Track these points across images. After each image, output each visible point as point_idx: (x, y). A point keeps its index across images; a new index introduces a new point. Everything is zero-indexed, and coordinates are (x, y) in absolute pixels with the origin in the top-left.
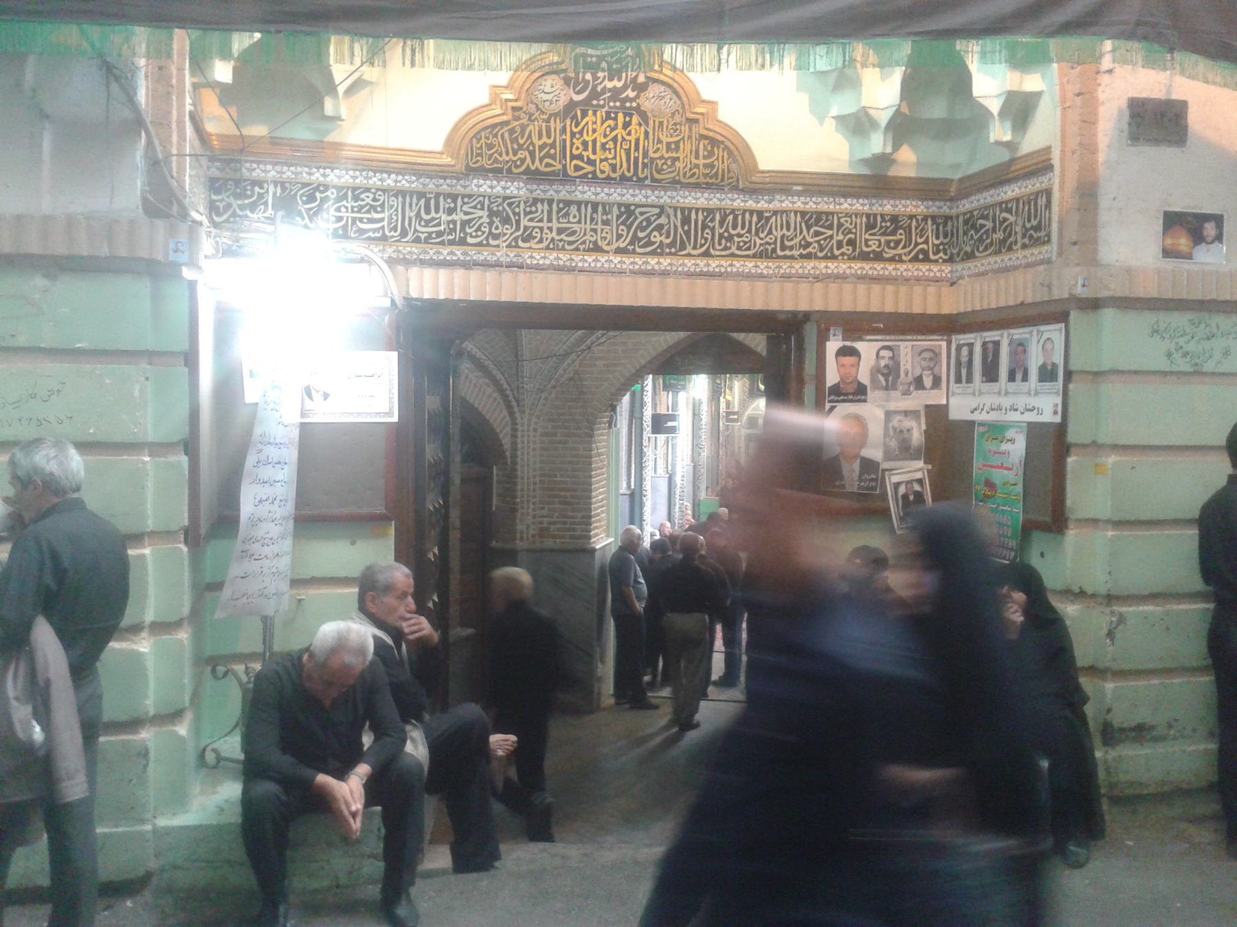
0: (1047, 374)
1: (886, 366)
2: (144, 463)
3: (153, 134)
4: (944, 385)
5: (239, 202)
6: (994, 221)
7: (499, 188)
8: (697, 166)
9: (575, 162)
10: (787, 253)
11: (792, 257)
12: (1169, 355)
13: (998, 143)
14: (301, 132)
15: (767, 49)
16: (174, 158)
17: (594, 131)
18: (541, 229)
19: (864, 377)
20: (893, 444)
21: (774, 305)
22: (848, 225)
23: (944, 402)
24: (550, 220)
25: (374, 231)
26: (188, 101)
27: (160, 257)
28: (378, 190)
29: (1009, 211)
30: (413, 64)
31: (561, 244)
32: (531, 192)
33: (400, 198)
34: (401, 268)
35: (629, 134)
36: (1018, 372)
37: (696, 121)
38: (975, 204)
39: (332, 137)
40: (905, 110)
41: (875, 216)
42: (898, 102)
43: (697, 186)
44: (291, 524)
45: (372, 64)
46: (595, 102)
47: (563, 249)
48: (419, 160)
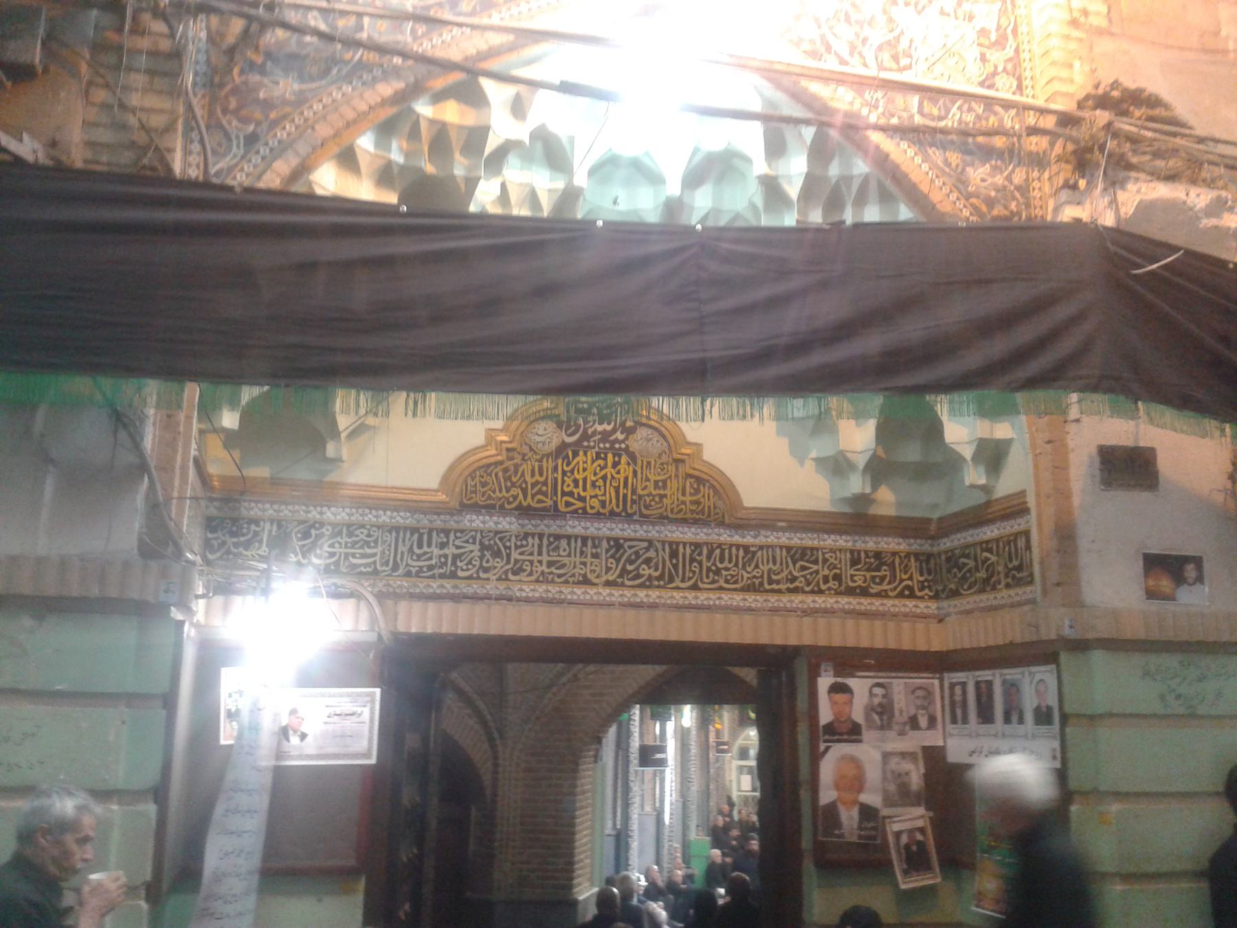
0: (1043, 716)
1: (880, 705)
2: (112, 811)
3: (156, 479)
4: (940, 726)
5: (235, 540)
6: (976, 560)
7: (491, 524)
8: (684, 503)
9: (565, 498)
10: (775, 586)
11: (779, 591)
12: (1162, 697)
13: (973, 486)
14: (303, 472)
15: (747, 402)
16: (174, 502)
17: (585, 470)
18: (531, 562)
19: (858, 715)
20: (892, 788)
21: (764, 639)
22: (832, 560)
23: (941, 743)
24: (540, 554)
25: (365, 565)
26: (194, 446)
27: (150, 598)
28: (372, 526)
29: (990, 551)
30: (414, 415)
31: (550, 577)
32: (523, 526)
33: (394, 534)
34: (390, 602)
35: (618, 472)
36: (1012, 713)
37: (683, 461)
38: (956, 543)
39: (332, 477)
40: (881, 453)
41: (859, 552)
42: (873, 446)
43: (684, 521)
44: (255, 880)
45: (376, 415)
46: (585, 444)
47: (553, 581)
48: (415, 498)
